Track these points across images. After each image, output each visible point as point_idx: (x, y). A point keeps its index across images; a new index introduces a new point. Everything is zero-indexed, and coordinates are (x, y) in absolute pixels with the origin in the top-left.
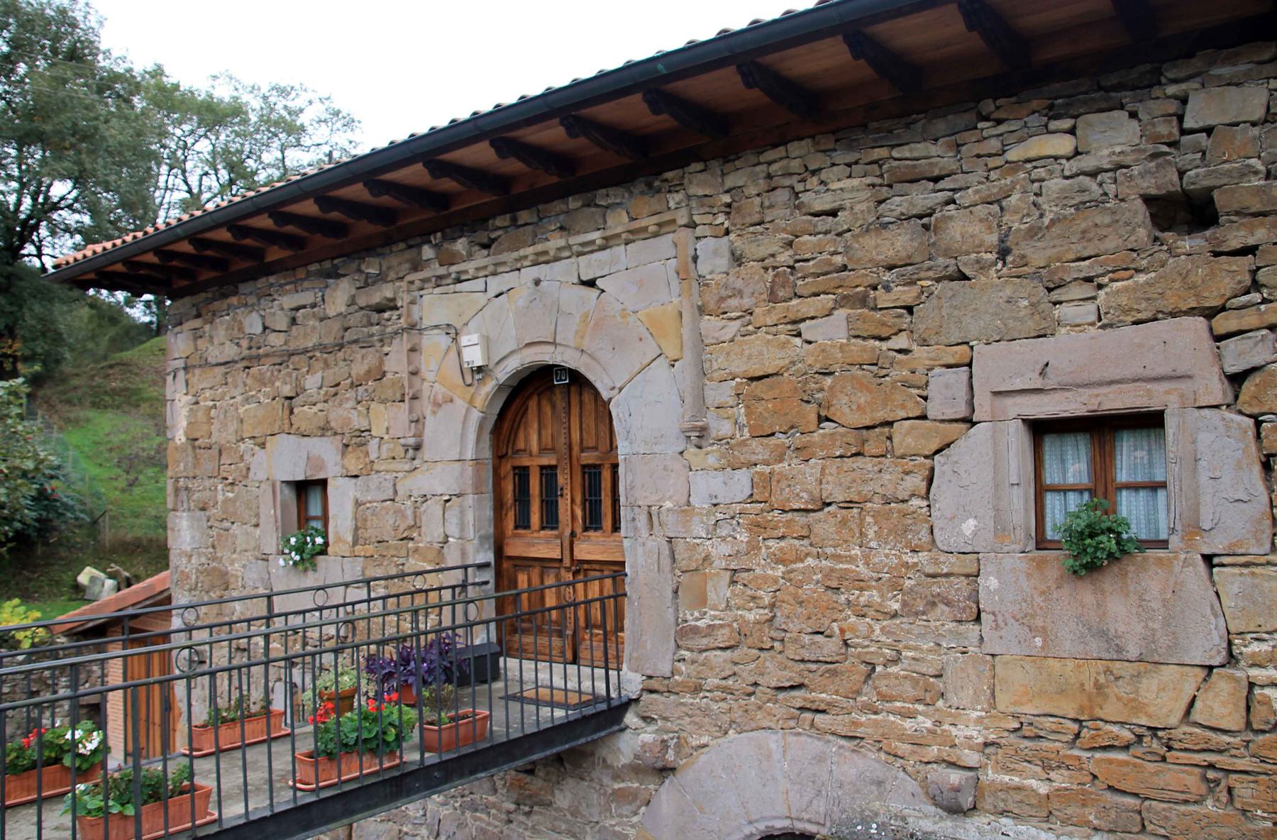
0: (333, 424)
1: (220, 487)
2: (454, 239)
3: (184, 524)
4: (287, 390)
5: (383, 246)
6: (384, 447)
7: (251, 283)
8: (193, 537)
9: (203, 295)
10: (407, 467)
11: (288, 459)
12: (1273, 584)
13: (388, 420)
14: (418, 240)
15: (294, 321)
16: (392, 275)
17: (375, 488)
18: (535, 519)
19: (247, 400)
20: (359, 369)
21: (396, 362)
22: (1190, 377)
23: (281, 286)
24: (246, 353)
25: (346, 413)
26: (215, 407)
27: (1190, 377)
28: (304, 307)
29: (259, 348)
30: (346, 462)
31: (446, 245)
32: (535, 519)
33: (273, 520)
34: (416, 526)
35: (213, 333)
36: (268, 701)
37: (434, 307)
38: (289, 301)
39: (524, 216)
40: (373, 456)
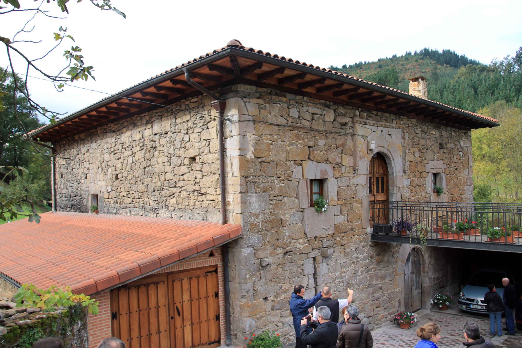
0: (330, 159)
1: (276, 181)
2: (364, 112)
3: (254, 199)
4: (311, 144)
5: (346, 105)
6: (347, 169)
7: (294, 96)
8: (260, 206)
9: (265, 90)
10: (353, 176)
11: (313, 170)
12: (165, 343)
13: (347, 161)
14: (356, 108)
15: (313, 119)
16: (348, 115)
17: (343, 182)
18: (380, 191)
19: (292, 144)
20: (339, 142)
21: (349, 143)
22: (74, 40)
23: (308, 102)
24: (290, 124)
25: (334, 156)
26: (271, 144)
27: (74, 40)
28: (317, 114)
29: (297, 123)
30: (335, 173)
31: (362, 113)
32: (380, 191)
33: (306, 194)
34: (355, 194)
35: (271, 110)
36: (416, 217)
37: (360, 129)
38: (312, 110)
39: (379, 113)
40: (343, 171)
